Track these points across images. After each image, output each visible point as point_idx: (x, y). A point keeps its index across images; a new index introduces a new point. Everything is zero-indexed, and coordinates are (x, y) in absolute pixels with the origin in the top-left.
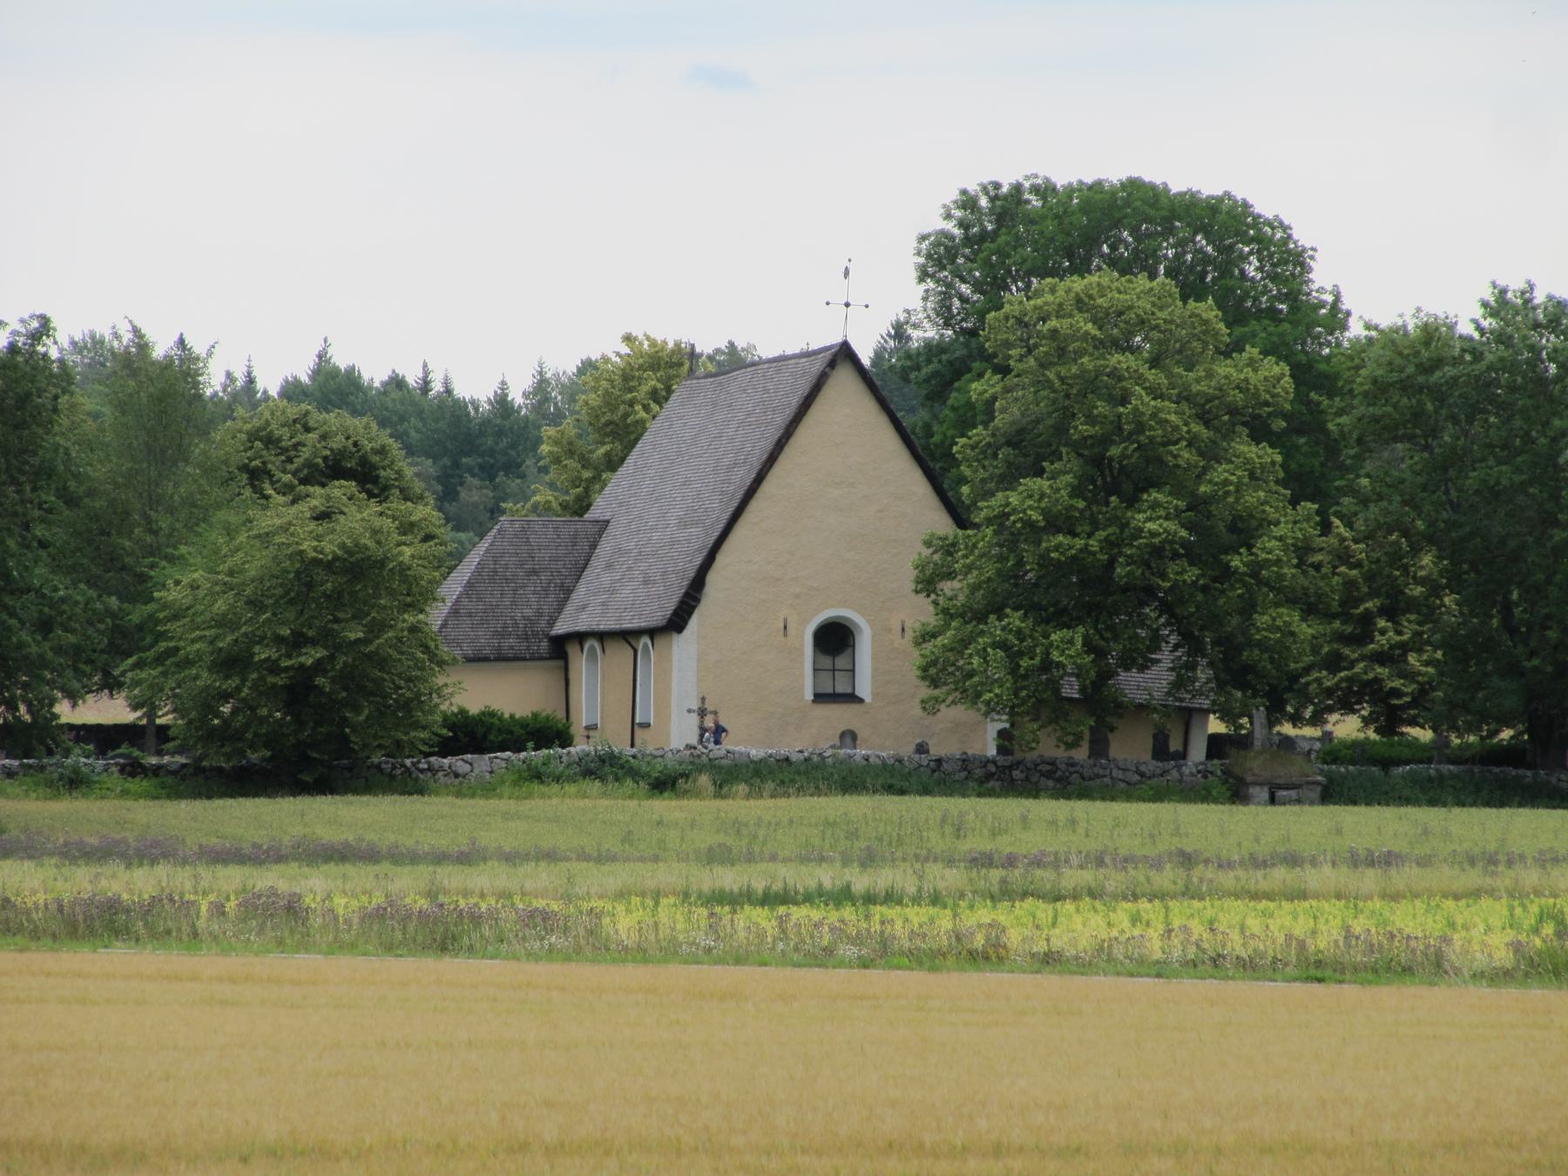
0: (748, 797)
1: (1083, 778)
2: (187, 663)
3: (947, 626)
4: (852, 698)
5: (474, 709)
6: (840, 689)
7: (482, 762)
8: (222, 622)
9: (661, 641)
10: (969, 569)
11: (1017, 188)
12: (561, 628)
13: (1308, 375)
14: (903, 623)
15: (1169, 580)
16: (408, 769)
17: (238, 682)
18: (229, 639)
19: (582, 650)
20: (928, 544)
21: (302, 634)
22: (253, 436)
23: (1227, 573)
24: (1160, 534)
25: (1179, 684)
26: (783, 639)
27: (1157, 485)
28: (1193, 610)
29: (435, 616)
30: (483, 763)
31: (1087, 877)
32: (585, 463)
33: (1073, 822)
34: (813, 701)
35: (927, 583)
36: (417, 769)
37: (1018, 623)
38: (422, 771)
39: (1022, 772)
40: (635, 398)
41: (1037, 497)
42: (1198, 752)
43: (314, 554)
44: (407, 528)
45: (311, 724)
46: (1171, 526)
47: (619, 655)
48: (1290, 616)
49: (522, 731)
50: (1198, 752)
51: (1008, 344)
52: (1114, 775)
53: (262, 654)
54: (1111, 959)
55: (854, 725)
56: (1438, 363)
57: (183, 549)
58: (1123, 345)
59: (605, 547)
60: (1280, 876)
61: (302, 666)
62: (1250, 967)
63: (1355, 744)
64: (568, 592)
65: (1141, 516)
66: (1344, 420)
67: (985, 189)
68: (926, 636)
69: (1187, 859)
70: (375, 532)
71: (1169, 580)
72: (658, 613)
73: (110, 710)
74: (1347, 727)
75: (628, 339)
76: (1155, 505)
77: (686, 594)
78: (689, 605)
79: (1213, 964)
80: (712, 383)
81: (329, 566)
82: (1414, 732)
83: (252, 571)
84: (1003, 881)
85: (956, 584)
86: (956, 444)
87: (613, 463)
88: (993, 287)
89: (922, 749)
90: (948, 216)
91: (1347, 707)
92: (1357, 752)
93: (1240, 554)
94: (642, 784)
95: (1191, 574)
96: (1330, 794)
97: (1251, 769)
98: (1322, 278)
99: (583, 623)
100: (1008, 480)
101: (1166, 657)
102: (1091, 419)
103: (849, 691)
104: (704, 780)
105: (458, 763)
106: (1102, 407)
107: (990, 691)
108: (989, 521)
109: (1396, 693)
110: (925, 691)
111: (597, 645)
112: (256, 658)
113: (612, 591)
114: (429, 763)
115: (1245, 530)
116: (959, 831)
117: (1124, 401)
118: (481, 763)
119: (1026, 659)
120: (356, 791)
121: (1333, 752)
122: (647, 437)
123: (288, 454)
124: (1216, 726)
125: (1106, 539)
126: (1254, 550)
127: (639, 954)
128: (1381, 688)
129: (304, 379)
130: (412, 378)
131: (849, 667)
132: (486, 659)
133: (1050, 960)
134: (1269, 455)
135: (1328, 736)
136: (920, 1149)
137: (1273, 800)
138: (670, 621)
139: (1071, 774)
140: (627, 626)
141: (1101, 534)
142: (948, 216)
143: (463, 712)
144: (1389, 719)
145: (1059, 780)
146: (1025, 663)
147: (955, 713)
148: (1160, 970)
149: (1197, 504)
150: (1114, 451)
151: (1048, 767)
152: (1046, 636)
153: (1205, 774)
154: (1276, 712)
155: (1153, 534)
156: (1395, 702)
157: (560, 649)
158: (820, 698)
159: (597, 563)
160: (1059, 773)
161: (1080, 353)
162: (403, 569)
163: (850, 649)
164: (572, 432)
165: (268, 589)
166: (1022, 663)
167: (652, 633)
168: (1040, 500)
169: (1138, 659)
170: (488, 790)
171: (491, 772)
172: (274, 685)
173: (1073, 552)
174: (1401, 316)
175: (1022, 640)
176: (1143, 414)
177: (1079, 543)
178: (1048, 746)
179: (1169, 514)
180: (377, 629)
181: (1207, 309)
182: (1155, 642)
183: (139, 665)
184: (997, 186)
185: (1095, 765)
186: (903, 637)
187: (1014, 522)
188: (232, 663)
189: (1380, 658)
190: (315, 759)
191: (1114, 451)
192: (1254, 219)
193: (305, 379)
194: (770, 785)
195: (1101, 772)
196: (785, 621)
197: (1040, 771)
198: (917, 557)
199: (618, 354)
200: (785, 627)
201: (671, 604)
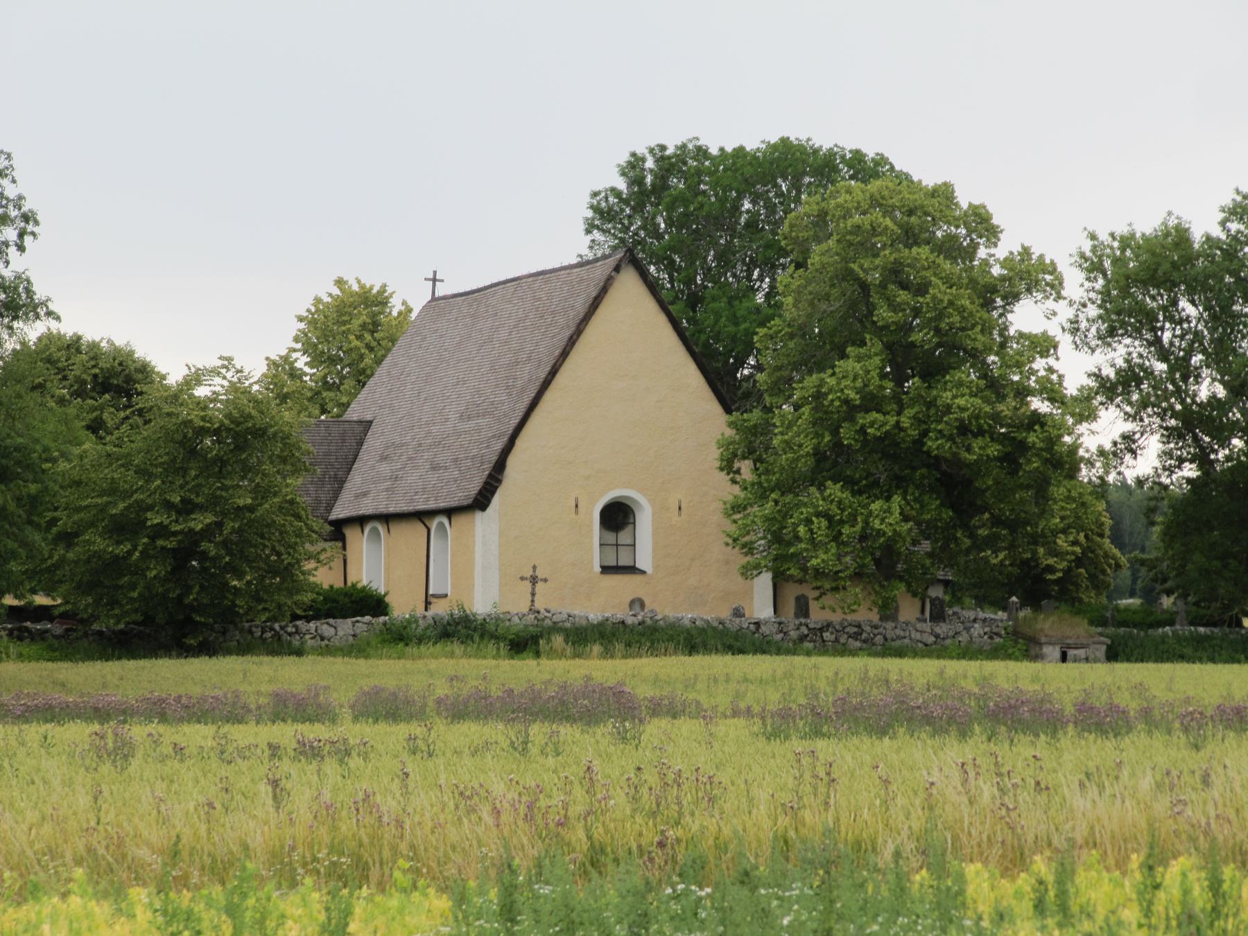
1: (886, 639)
4: (632, 570)
6: (624, 561)
9: (461, 521)
12: (338, 513)
14: (680, 502)
15: (974, 453)
16: (277, 633)
17: (129, 547)
18: (121, 506)
19: (363, 532)
21: (190, 501)
24: (968, 409)
26: (573, 516)
28: (990, 483)
30: (346, 627)
34: (602, 573)
36: (286, 632)
37: (839, 494)
38: (290, 634)
39: (832, 633)
40: (349, 330)
41: (851, 377)
43: (202, 424)
45: (197, 589)
47: (415, 531)
49: (347, 600)
52: (913, 636)
53: (154, 519)
55: (640, 594)
59: (373, 443)
61: (191, 530)
65: (949, 394)
67: (651, 151)
71: (974, 453)
75: (340, 282)
77: (490, 476)
78: (491, 485)
80: (464, 301)
86: (757, 333)
93: (1035, 431)
94: (502, 645)
97: (1042, 630)
99: (367, 507)
102: (894, 307)
103: (632, 564)
104: (558, 640)
107: (816, 557)
111: (445, 521)
112: (149, 523)
114: (296, 627)
118: (345, 627)
119: (847, 527)
125: (914, 417)
126: (1046, 428)
128: (1038, 565)
131: (629, 541)
138: (476, 500)
139: (875, 635)
140: (421, 507)
145: (865, 641)
151: (856, 630)
152: (866, 506)
155: (963, 409)
156: (1049, 577)
158: (606, 570)
160: (864, 636)
163: (630, 527)
165: (156, 459)
166: (843, 531)
167: (450, 512)
168: (855, 379)
171: (354, 636)
172: (163, 548)
173: (888, 428)
174: (1130, 225)
175: (843, 510)
176: (942, 301)
179: (972, 391)
180: (262, 493)
184: (663, 148)
185: (896, 627)
186: (680, 515)
187: (832, 401)
190: (199, 623)
194: (619, 647)
195: (902, 633)
196: (577, 500)
197: (847, 633)
198: (720, 437)
199: (330, 295)
200: (577, 506)
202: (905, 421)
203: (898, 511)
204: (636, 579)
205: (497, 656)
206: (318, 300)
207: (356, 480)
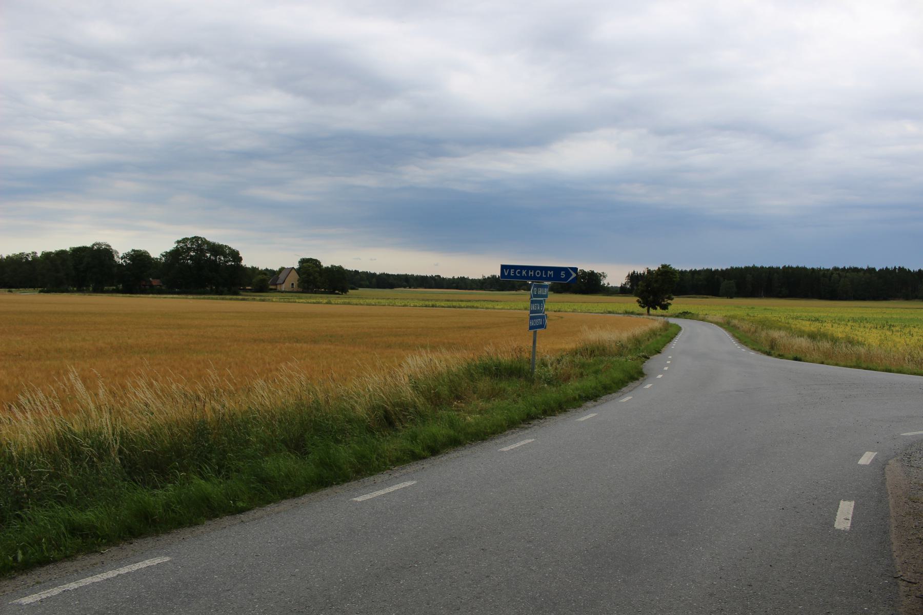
62: (340, 304)
72: (282, 282)
73: (250, 288)
88: (303, 264)
98: (322, 264)
129: (877, 270)
133: (299, 302)
136: (854, 320)
144: (325, 289)
181: (315, 266)
193: (781, 268)
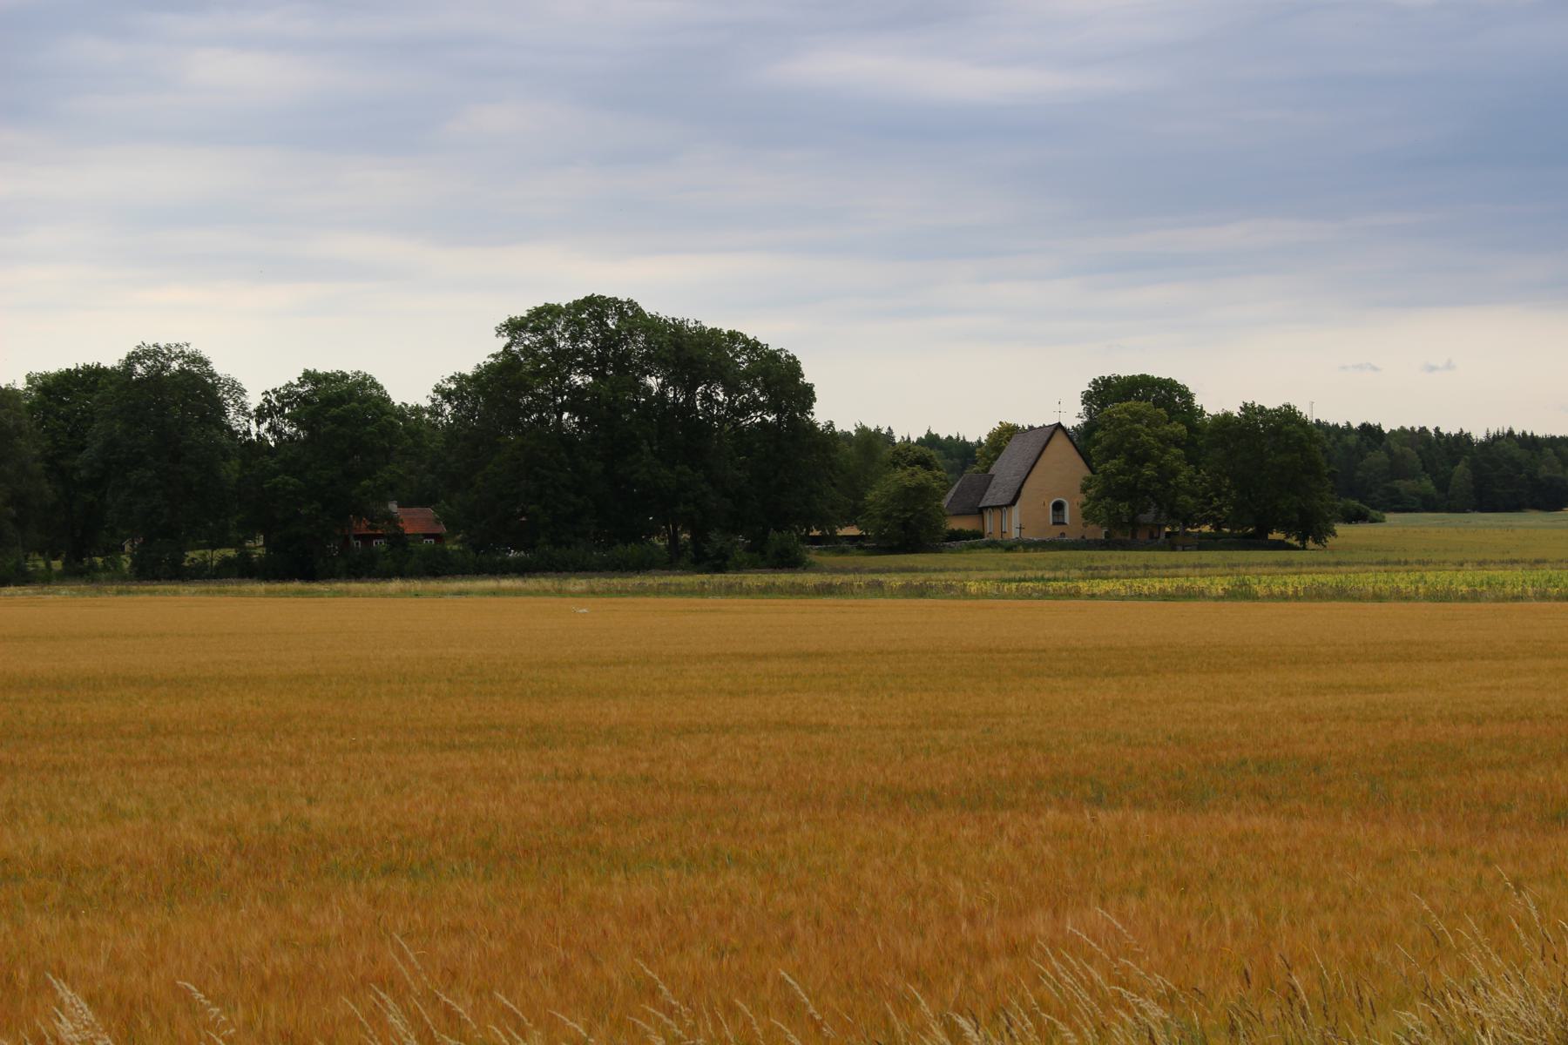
0: (1033, 552)
2: (874, 517)
3: (1089, 503)
5: (956, 529)
7: (958, 543)
8: (884, 506)
10: (1095, 486)
11: (1109, 378)
12: (981, 506)
13: (1192, 429)
18: (886, 510)
20: (1084, 479)
22: (894, 453)
23: (1169, 485)
25: (1156, 518)
27: (1148, 461)
29: (944, 503)
31: (1115, 572)
32: (989, 459)
33: (1125, 558)
35: (1084, 490)
42: (1163, 537)
44: (935, 478)
46: (1153, 473)
48: (1188, 498)
50: (1163, 537)
51: (1105, 422)
53: (895, 514)
54: (1110, 596)
56: (1228, 425)
57: (874, 486)
58: (1139, 421)
59: (993, 482)
60: (1171, 571)
63: (1207, 533)
64: (983, 495)
66: (1202, 441)
68: (1083, 505)
69: (1127, 568)
70: (926, 479)
72: (1008, 500)
73: (853, 531)
74: (1206, 529)
75: (1001, 423)
76: (1148, 467)
79: (1139, 596)
81: (913, 489)
82: (1226, 530)
83: (892, 490)
84: (1092, 574)
85: (1092, 490)
87: (996, 458)
89: (1083, 537)
90: (1090, 386)
91: (1205, 523)
92: (1208, 535)
95: (1159, 486)
96: (1200, 548)
98: (1197, 402)
99: (987, 504)
100: (1106, 460)
101: (1152, 509)
105: (951, 544)
106: (1132, 439)
108: (1101, 472)
109: (1220, 519)
110: (1084, 521)
113: (995, 495)
115: (1174, 473)
116: (1092, 560)
117: (1139, 437)
120: (923, 553)
121: (1201, 536)
122: (1005, 451)
123: (904, 458)
124: (1167, 529)
127: (977, 597)
130: (954, 437)
132: (961, 514)
133: (1093, 596)
134: (1179, 452)
135: (1200, 531)
137: (1183, 550)
141: (1133, 475)
142: (1090, 386)
143: (953, 529)
144: (1218, 527)
146: (1112, 512)
147: (1092, 527)
148: (1123, 598)
149: (1160, 466)
150: (1136, 452)
153: (1164, 542)
154: (1186, 524)
155: (1148, 475)
157: (981, 511)
158: (1054, 523)
159: (991, 486)
161: (1126, 424)
162: (934, 489)
164: (984, 450)
167: (1006, 506)
169: (1144, 510)
170: (960, 551)
177: (1126, 478)
178: (1118, 536)
182: (1149, 504)
183: (862, 518)
184: (1104, 377)
188: (887, 517)
189: (1214, 509)
191: (1136, 452)
192: (621, 313)
193: (923, 437)
201: (1011, 498)
202: (1131, 478)
203: (1189, 498)
204: (1064, 526)
205: (1001, 552)
206: (994, 429)
207: (991, 490)
